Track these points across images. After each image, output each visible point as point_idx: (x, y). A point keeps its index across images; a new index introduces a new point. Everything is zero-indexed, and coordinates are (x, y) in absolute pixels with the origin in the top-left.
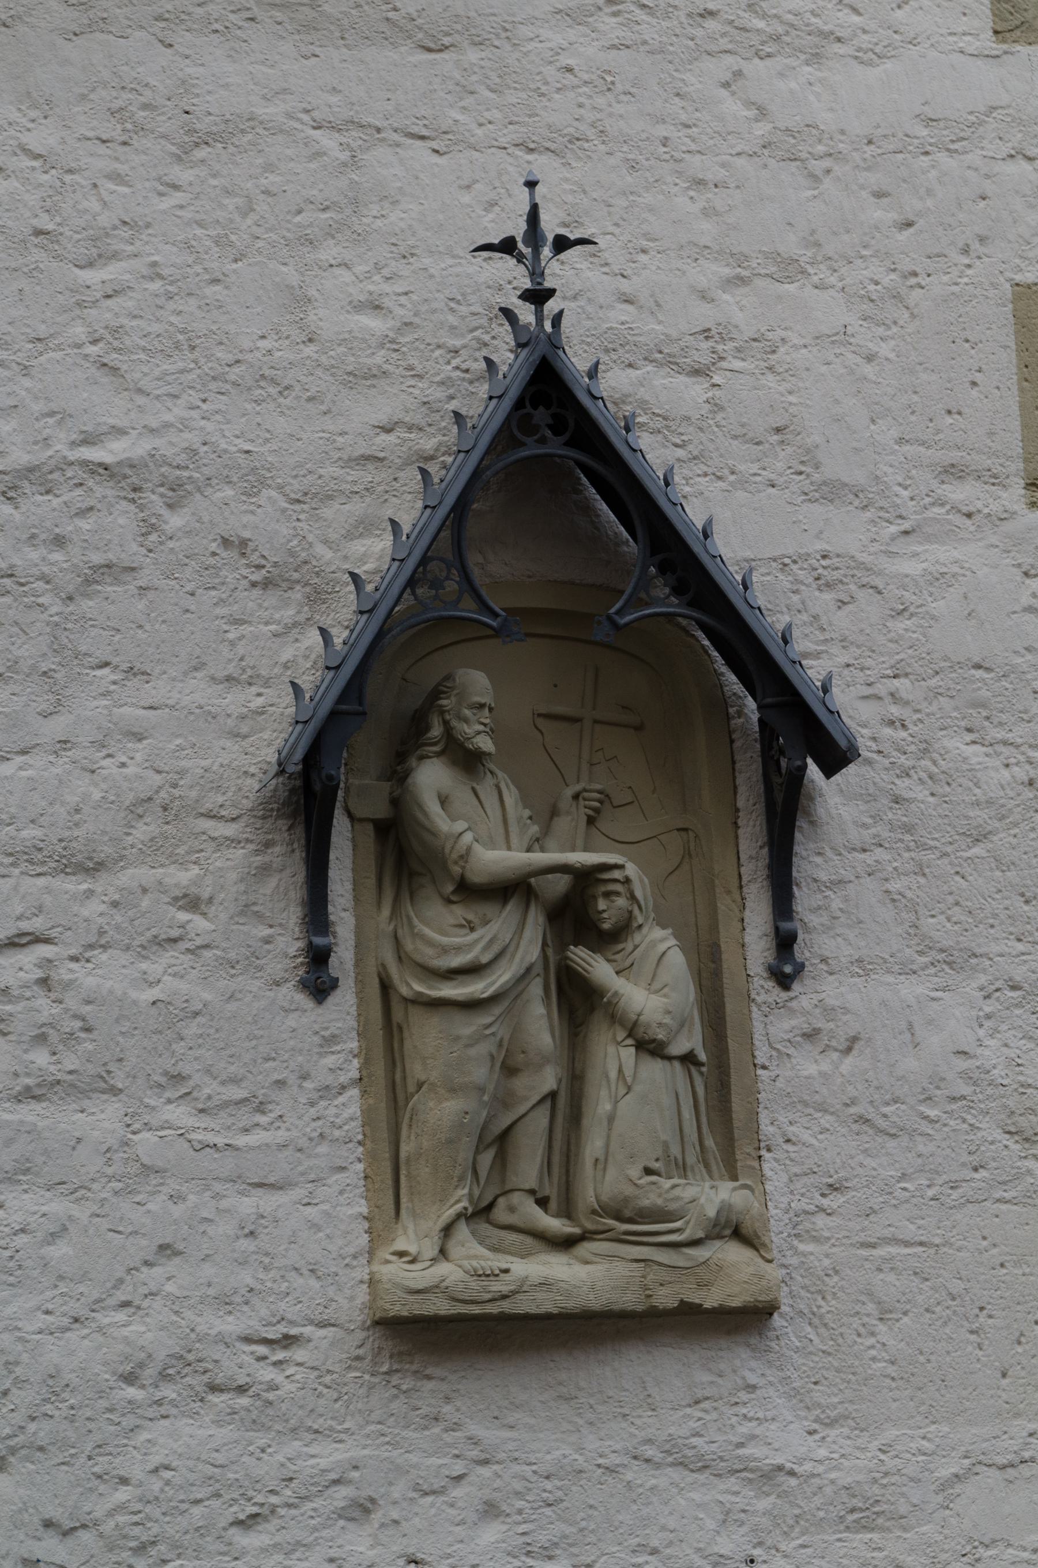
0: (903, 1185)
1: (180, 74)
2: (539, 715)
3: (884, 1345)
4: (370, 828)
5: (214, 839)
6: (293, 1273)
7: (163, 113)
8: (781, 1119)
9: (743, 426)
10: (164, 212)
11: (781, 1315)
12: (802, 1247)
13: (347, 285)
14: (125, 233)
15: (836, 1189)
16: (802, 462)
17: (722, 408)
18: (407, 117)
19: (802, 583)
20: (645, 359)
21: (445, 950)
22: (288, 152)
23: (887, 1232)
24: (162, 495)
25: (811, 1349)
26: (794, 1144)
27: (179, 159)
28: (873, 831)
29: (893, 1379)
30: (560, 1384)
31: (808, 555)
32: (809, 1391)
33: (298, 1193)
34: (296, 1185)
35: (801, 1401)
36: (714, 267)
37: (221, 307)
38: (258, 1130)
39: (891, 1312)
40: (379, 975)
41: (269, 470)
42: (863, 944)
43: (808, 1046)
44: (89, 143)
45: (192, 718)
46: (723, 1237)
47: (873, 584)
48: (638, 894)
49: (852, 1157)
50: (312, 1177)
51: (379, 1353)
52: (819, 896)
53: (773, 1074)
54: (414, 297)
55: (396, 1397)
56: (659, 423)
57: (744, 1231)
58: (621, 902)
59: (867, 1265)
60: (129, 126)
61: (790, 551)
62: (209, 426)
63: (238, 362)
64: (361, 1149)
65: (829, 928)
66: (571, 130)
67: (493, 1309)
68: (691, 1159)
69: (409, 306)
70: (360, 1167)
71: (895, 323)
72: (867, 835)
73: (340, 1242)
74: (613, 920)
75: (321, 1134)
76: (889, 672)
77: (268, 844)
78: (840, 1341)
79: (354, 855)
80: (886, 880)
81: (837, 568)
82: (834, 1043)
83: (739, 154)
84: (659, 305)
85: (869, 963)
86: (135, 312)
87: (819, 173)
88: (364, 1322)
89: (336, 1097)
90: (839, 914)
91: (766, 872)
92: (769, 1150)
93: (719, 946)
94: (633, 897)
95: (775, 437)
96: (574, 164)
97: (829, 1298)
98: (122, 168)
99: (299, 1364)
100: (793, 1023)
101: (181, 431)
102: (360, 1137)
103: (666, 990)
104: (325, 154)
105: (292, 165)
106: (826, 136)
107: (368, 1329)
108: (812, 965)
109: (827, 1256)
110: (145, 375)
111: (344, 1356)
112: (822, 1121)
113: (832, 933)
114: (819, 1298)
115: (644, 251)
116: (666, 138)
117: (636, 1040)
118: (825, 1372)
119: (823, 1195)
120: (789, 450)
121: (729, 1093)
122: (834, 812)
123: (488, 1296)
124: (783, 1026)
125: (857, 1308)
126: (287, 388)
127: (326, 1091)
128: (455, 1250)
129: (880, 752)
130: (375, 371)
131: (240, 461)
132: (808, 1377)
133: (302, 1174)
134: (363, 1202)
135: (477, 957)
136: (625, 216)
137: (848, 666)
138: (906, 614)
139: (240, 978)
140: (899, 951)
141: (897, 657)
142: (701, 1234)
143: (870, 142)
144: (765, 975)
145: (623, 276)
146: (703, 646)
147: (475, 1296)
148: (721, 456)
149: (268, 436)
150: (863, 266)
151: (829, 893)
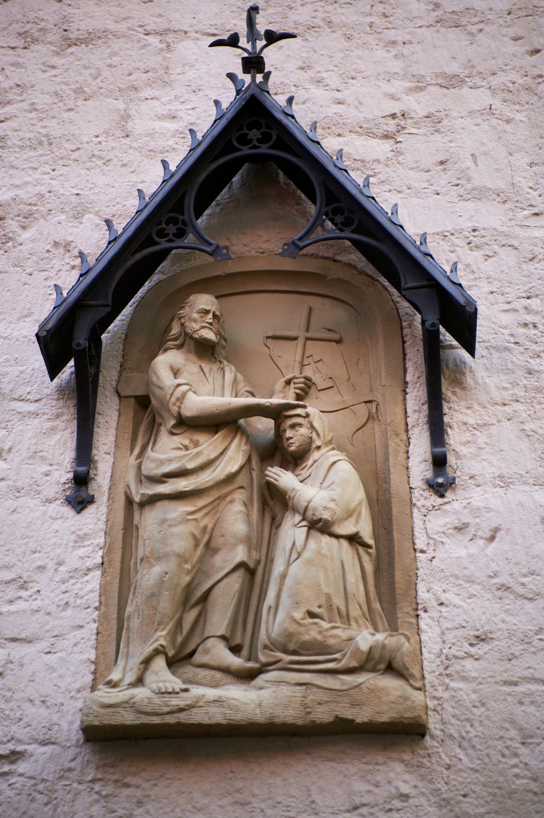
0: (540, 637)
1: (64, 13)
2: (268, 337)
3: (526, 764)
4: (133, 400)
5: (20, 413)
6: (28, 704)
7: (51, 32)
8: (435, 587)
9: (417, 162)
10: (44, 79)
11: (432, 737)
12: (453, 684)
13: (156, 107)
14: (18, 91)
15: (483, 640)
16: (458, 179)
17: (402, 154)
18: (204, 25)
19: (457, 246)
20: (350, 131)
21: (162, 463)
22: (126, 46)
23: (527, 673)
24: (19, 221)
25: (460, 766)
26: (447, 606)
27: (58, 54)
28: (512, 392)
29: (535, 794)
30: (237, 791)
31: (463, 230)
32: (458, 803)
33: (43, 645)
34: (42, 639)
35: (451, 811)
36: (400, 83)
37: (72, 122)
38: (20, 602)
39: (532, 737)
40: (126, 494)
41: (90, 203)
42: (504, 465)
43: (459, 537)
44: (3, 49)
45: (18, 343)
46: (379, 670)
47: (510, 244)
48: (316, 424)
49: (495, 616)
50: (55, 633)
51: (87, 765)
52: (468, 434)
53: (430, 556)
54: (197, 110)
55: (97, 801)
56: (359, 164)
57: (396, 665)
58: (303, 431)
59: (510, 699)
60: (29, 39)
61: (450, 229)
62: (54, 183)
63: (78, 149)
64: (97, 613)
65: (476, 456)
66: (310, 23)
67: (171, 720)
68: (355, 612)
69: (194, 115)
70: (96, 625)
71: (527, 103)
72: (507, 395)
73: (69, 680)
74: (297, 444)
75: (67, 603)
76: (524, 295)
77: (58, 416)
78: (486, 760)
79: (119, 420)
80: (522, 423)
81: (484, 236)
82: (480, 533)
83: (420, 27)
84: (360, 103)
85: (509, 478)
86: (17, 128)
87: (475, 32)
88: (78, 741)
89: (82, 577)
90: (484, 445)
91: (426, 419)
92: (426, 611)
93: (389, 470)
94: (312, 427)
95: (440, 167)
96: (310, 39)
97: (476, 724)
98: (20, 60)
99: (21, 775)
100: (446, 520)
101: (35, 186)
102: (97, 604)
103: (332, 486)
104: (150, 45)
105: (129, 51)
106: (479, 12)
107: (81, 746)
108: (462, 480)
109: (475, 691)
110: (17, 158)
111: (59, 768)
112: (470, 589)
113: (479, 459)
114: (468, 725)
115: (353, 78)
116: (372, 23)
117: (308, 522)
118: (473, 787)
119: (471, 645)
120: (450, 173)
121: (394, 570)
122: (480, 381)
123: (167, 709)
124: (437, 523)
125: (501, 733)
126: (108, 161)
127: (75, 573)
128: (149, 678)
129: (516, 343)
130: (167, 148)
131: (72, 200)
132: (457, 790)
133: (47, 631)
134: (94, 651)
135: (184, 464)
136: (342, 62)
137: (492, 293)
138: (536, 260)
139: (23, 498)
140: (533, 469)
141: (530, 285)
142: (354, 664)
143: (509, 13)
144: (425, 487)
145: (338, 91)
146: (384, 286)
147: (157, 709)
148: (401, 179)
149: (93, 186)
150: (505, 75)
151: (475, 432)
